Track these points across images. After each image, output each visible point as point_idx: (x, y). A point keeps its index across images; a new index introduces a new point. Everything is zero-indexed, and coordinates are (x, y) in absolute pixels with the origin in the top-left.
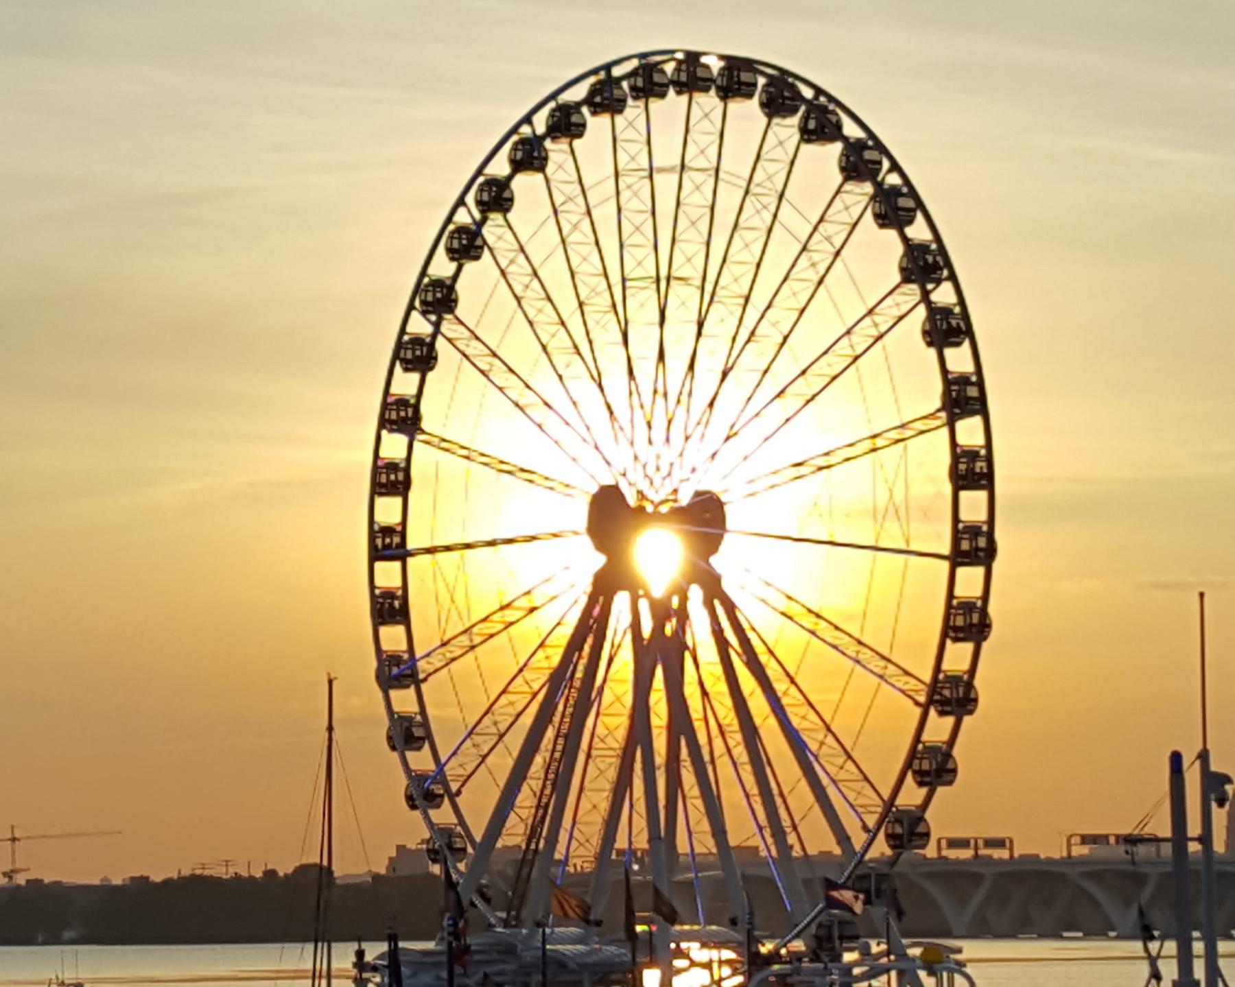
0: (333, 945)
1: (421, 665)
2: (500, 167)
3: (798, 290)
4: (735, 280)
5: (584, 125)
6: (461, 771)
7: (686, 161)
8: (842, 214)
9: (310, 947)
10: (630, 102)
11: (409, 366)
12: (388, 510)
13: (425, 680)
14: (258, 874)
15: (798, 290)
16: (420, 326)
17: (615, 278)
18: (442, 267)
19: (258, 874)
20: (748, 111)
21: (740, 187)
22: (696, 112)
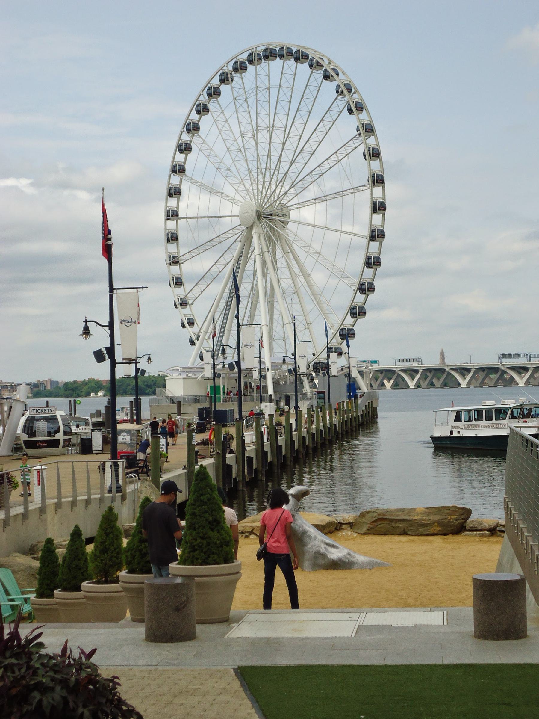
0: (538, 546)
1: (182, 258)
2: (216, 82)
3: (320, 134)
4: (295, 132)
5: (246, 67)
6: (193, 296)
7: (281, 84)
8: (336, 108)
9: (86, 491)
10: (263, 60)
11: (181, 151)
12: (172, 203)
13: (182, 263)
14: (156, 375)
15: (320, 134)
16: (186, 137)
17: (254, 126)
18: (194, 116)
19: (156, 375)
20: (304, 67)
21: (48, 498)
22: (286, 66)
